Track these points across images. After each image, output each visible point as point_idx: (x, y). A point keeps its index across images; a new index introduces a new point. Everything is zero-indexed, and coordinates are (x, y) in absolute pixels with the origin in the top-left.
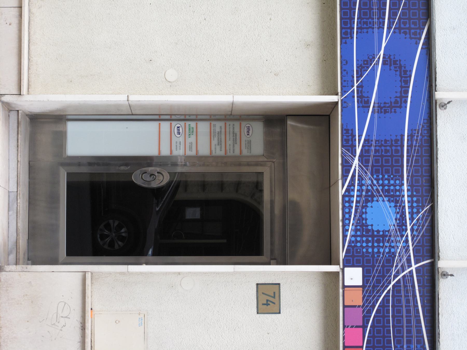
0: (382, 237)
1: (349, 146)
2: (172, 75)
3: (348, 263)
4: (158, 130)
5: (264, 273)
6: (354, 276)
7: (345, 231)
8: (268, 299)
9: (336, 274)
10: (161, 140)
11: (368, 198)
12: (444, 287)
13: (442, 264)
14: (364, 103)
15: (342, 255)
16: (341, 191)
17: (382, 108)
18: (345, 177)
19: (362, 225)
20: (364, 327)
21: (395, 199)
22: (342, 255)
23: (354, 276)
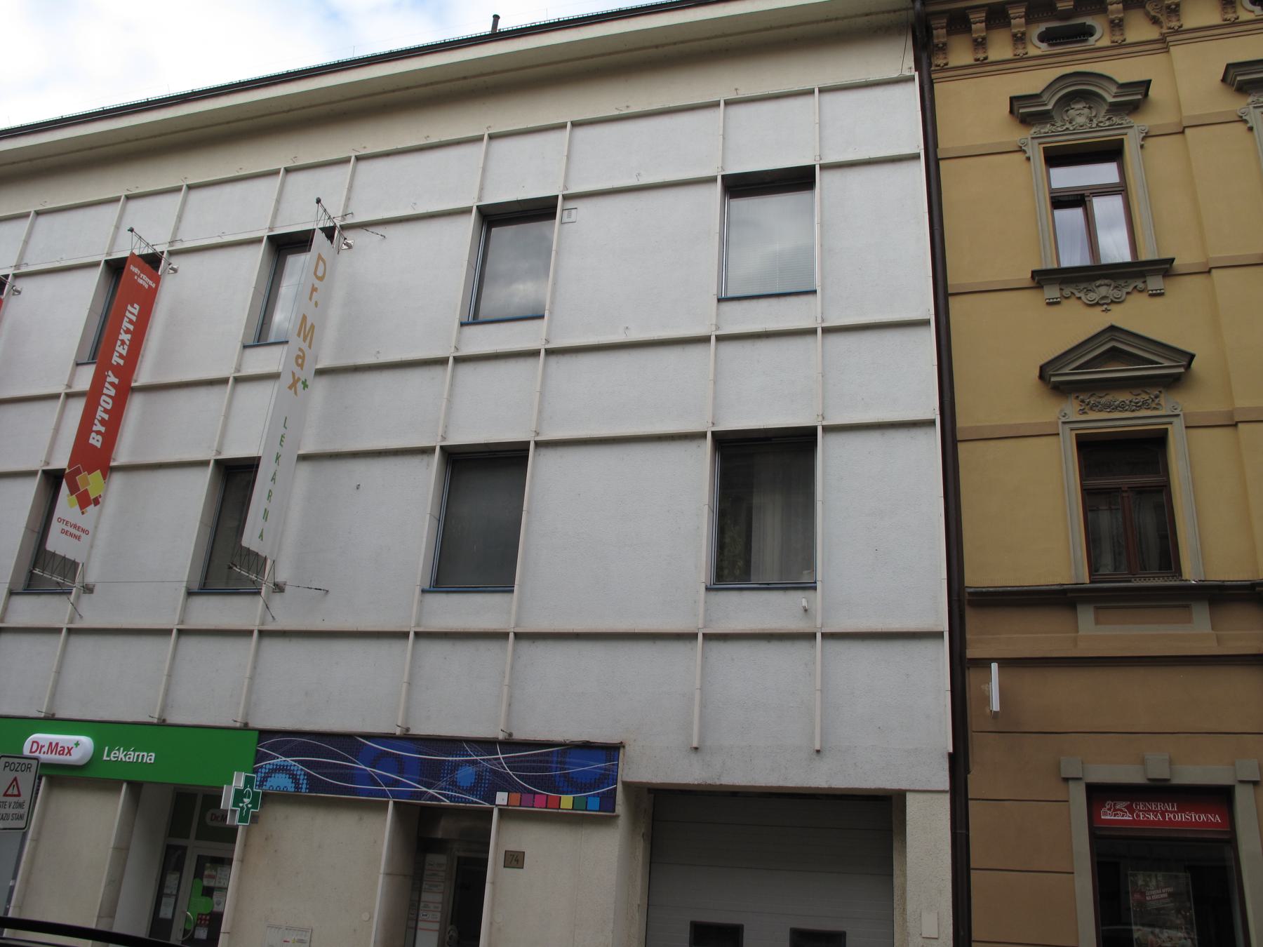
0: (479, 776)
1: (421, 795)
2: (365, 916)
3: (493, 801)
4: (764, 303)
5: (495, 864)
6: (502, 798)
7: (473, 802)
8: (515, 860)
9: (500, 810)
10: (746, 304)
11: (454, 785)
12: (519, 735)
13: (501, 736)
14: (396, 783)
15: (487, 805)
16: (447, 803)
17: (400, 772)
18: (440, 800)
19: (471, 790)
20: (535, 793)
21: (457, 766)
22: (487, 805)
23: (502, 798)
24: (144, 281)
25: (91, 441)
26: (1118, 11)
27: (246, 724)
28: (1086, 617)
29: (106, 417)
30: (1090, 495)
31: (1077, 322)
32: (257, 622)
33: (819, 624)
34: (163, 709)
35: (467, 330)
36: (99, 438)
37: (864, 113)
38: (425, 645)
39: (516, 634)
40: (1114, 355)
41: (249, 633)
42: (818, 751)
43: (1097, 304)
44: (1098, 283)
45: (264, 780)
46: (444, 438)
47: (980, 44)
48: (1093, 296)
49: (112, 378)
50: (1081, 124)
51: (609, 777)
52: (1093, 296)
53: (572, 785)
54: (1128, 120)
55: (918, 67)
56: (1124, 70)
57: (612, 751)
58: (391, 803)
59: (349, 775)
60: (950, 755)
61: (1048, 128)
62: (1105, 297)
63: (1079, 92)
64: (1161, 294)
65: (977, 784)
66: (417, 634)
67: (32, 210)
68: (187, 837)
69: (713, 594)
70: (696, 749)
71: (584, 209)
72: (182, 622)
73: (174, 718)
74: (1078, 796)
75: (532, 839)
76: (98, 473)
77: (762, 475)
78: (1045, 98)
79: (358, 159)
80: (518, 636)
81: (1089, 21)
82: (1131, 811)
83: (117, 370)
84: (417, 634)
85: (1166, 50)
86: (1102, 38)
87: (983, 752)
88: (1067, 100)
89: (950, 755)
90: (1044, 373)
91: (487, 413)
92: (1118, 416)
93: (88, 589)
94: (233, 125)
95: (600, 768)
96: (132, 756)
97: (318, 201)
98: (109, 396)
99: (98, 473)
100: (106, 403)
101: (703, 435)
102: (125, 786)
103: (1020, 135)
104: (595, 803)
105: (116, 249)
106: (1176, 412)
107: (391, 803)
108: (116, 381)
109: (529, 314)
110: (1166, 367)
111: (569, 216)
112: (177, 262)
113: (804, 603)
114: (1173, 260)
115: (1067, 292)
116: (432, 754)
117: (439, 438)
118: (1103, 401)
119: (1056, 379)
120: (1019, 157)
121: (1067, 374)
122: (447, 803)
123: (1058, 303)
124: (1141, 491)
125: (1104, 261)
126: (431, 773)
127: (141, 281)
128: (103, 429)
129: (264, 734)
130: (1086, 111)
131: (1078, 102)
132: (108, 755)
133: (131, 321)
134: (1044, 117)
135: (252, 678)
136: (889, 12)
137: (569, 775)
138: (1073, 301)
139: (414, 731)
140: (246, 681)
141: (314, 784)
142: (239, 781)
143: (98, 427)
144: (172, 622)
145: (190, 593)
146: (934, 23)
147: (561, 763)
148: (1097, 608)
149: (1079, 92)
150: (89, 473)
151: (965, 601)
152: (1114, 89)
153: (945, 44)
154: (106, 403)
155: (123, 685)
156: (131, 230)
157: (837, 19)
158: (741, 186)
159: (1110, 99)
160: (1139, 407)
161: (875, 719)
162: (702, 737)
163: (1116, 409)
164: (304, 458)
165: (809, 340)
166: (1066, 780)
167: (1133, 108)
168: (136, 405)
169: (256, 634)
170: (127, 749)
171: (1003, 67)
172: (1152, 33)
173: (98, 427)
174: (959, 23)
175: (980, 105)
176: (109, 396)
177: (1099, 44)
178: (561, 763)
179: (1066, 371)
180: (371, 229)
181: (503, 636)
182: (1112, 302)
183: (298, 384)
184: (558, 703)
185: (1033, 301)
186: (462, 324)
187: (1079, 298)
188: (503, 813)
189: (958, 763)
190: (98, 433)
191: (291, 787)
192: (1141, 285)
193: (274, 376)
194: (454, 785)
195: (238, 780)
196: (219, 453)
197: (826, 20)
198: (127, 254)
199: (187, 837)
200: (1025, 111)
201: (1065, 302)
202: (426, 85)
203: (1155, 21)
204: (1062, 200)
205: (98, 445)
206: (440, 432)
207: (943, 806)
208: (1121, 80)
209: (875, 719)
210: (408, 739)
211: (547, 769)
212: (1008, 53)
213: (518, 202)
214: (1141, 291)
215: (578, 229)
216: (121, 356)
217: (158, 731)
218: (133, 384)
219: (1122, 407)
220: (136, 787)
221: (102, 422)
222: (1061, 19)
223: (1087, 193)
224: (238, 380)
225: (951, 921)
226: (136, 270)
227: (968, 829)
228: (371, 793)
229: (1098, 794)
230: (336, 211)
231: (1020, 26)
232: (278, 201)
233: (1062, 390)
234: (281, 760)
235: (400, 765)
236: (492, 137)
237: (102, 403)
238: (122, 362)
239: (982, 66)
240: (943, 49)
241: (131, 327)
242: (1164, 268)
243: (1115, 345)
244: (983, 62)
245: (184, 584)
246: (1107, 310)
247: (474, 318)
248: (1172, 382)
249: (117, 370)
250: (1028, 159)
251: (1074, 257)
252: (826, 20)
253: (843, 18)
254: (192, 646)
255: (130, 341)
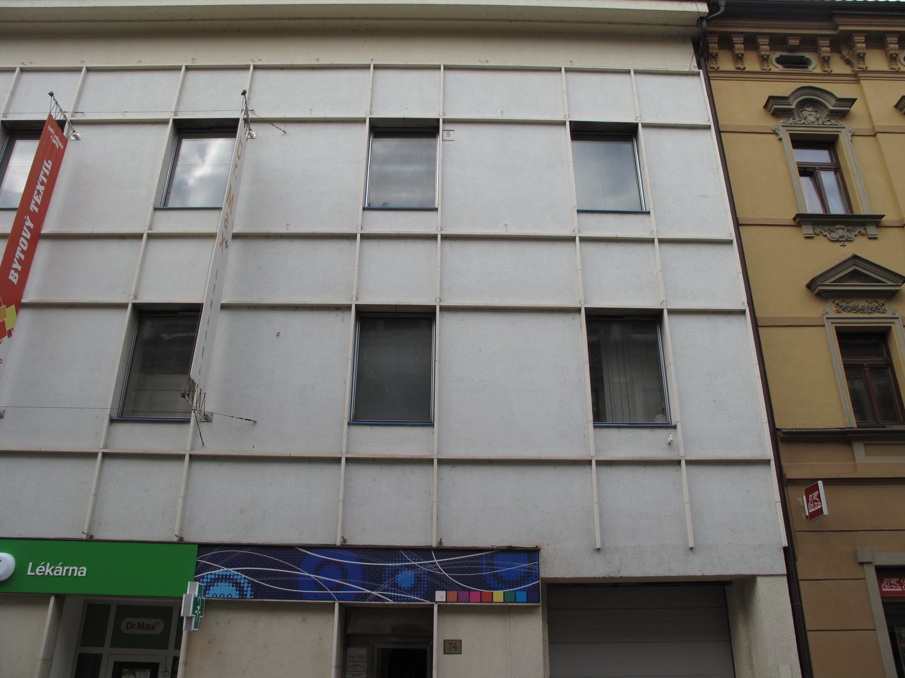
0: (418, 578)
1: (365, 596)
3: (432, 598)
5: (437, 649)
6: (440, 596)
7: (414, 600)
8: (453, 647)
10: (597, 216)
11: (396, 587)
12: (447, 543)
13: (434, 545)
14: (341, 587)
15: (428, 602)
16: (391, 602)
17: (344, 577)
19: (411, 591)
20: (465, 589)
21: (397, 570)
22: (428, 602)
23: (440, 596)
24: (56, 141)
25: (11, 277)
26: (827, 52)
27: (181, 539)
28: (859, 450)
29: (23, 257)
30: (847, 367)
31: (826, 254)
32: (188, 448)
33: (684, 454)
34: (90, 528)
35: (159, 213)
36: (16, 275)
37: (666, 94)
38: (355, 469)
39: (438, 460)
40: (855, 275)
41: (181, 457)
42: (691, 549)
43: (837, 241)
44: (837, 227)
45: (207, 588)
46: (135, 298)
47: (739, 58)
48: (835, 235)
49: (29, 223)
50: (812, 122)
51: (532, 574)
52: (835, 235)
53: (502, 582)
54: (841, 123)
55: (700, 67)
56: (842, 90)
57: (533, 553)
58: (337, 605)
59: (295, 582)
60: (785, 549)
61: (791, 121)
62: (842, 237)
63: (811, 100)
64: (876, 238)
65: (803, 570)
66: (347, 459)
67: (18, 66)
68: (102, 645)
69: (598, 430)
70: (599, 549)
71: (459, 132)
72: (106, 447)
73: (101, 535)
74: (871, 575)
75: (469, 630)
76: (13, 307)
77: (624, 342)
78: (791, 100)
79: (23, 70)
80: (441, 462)
81: (807, 55)
82: (901, 585)
83: (33, 216)
84: (347, 459)
85: (857, 81)
86: (815, 67)
87: (806, 547)
88: (803, 104)
89: (785, 549)
90: (810, 286)
91: (396, 280)
92: (861, 316)
93: (207, 419)
94: (292, 22)
95: (524, 568)
96: (61, 571)
97: (51, 94)
98: (26, 238)
99: (13, 307)
100: (23, 245)
101: (348, 308)
102: (52, 600)
103: (771, 123)
104: (522, 596)
105: (181, 108)
106: (896, 316)
107: (337, 605)
108: (32, 226)
109: (416, 206)
110: (888, 285)
111: (449, 135)
112: (80, 131)
113: (671, 438)
114: (883, 216)
115: (818, 230)
116: (375, 562)
117: (132, 297)
118: (851, 305)
119: (818, 289)
120: (773, 137)
121: (828, 285)
122: (391, 602)
123: (812, 238)
124: (875, 368)
125: (856, 213)
126: (373, 578)
127: (54, 141)
128: (19, 268)
129: (203, 547)
130: (814, 113)
131: (808, 107)
132: (33, 570)
133: (45, 175)
134: (787, 113)
135: (185, 498)
136: (680, 26)
137: (498, 574)
138: (821, 238)
139: (352, 542)
140: (181, 500)
141: (258, 591)
142: (193, 590)
143: (16, 265)
144: (98, 446)
145: (112, 421)
146: (709, 39)
147: (489, 564)
148: (865, 445)
149: (811, 100)
150: (7, 307)
151: (782, 438)
152: (833, 101)
153: (717, 54)
154: (23, 245)
155: (54, 505)
156: (51, 94)
157: (644, 24)
158: (382, 129)
159: (831, 108)
160: (873, 311)
161: (734, 526)
162: (602, 541)
163: (859, 311)
164: (224, 307)
165: (647, 248)
166: (862, 564)
167: (842, 115)
168: (43, 248)
169: (187, 458)
170: (54, 563)
171: (754, 76)
172: (847, 70)
173: (16, 265)
174: (726, 42)
175: (748, 97)
176: (26, 238)
177: (815, 71)
178: (489, 564)
179: (828, 283)
180: (276, 125)
181: (430, 462)
182: (847, 240)
183: (224, 244)
184: (481, 516)
185: (794, 236)
186: (156, 209)
187: (825, 236)
188: (443, 609)
189: (789, 553)
190: (16, 270)
191: (235, 594)
192: (863, 231)
193: (211, 236)
194: (396, 587)
195: (193, 588)
196: (135, 298)
197: (637, 24)
198: (44, 117)
199: (102, 645)
200: (776, 108)
201: (816, 237)
202: (318, 19)
203: (848, 62)
204: (806, 171)
205: (15, 281)
206: (133, 291)
207: (783, 585)
208: (839, 96)
209: (734, 526)
210: (346, 549)
211: (478, 570)
212: (757, 68)
213: (405, 119)
214: (863, 235)
215: (452, 145)
216: (36, 204)
217: (87, 546)
218: (43, 232)
219: (862, 310)
220: (61, 599)
221: (20, 260)
222: (789, 51)
223: (817, 167)
224: (151, 237)
225: (800, 671)
226: (52, 131)
227: (801, 602)
228: (316, 597)
229: (884, 572)
230: (67, 108)
231: (863, 49)
232: (181, 92)
233: (823, 296)
234: (223, 570)
235: (344, 572)
236: (256, 68)
237: (21, 244)
238: (37, 210)
239: (741, 74)
240: (715, 57)
241: (45, 180)
242: (875, 220)
243: (857, 269)
244: (742, 71)
245: (108, 411)
246: (844, 246)
247: (163, 207)
248: (891, 296)
249: (33, 216)
250: (780, 139)
251: (813, 207)
252: (637, 24)
253: (649, 24)
254: (116, 468)
255: (45, 192)
